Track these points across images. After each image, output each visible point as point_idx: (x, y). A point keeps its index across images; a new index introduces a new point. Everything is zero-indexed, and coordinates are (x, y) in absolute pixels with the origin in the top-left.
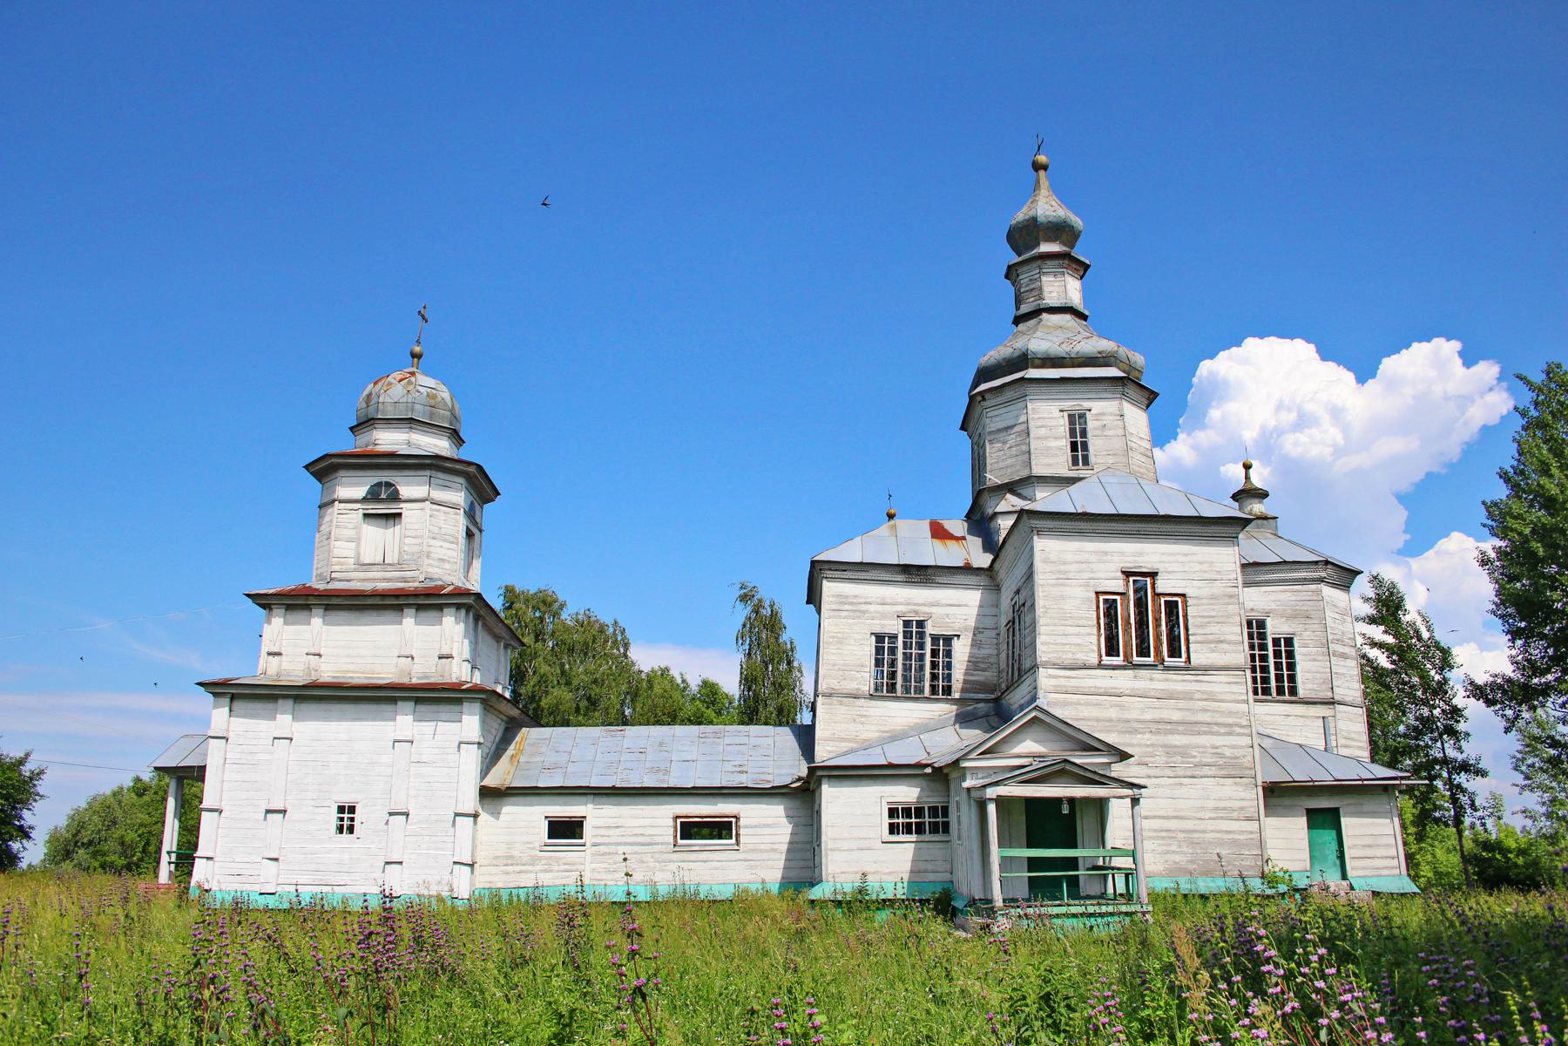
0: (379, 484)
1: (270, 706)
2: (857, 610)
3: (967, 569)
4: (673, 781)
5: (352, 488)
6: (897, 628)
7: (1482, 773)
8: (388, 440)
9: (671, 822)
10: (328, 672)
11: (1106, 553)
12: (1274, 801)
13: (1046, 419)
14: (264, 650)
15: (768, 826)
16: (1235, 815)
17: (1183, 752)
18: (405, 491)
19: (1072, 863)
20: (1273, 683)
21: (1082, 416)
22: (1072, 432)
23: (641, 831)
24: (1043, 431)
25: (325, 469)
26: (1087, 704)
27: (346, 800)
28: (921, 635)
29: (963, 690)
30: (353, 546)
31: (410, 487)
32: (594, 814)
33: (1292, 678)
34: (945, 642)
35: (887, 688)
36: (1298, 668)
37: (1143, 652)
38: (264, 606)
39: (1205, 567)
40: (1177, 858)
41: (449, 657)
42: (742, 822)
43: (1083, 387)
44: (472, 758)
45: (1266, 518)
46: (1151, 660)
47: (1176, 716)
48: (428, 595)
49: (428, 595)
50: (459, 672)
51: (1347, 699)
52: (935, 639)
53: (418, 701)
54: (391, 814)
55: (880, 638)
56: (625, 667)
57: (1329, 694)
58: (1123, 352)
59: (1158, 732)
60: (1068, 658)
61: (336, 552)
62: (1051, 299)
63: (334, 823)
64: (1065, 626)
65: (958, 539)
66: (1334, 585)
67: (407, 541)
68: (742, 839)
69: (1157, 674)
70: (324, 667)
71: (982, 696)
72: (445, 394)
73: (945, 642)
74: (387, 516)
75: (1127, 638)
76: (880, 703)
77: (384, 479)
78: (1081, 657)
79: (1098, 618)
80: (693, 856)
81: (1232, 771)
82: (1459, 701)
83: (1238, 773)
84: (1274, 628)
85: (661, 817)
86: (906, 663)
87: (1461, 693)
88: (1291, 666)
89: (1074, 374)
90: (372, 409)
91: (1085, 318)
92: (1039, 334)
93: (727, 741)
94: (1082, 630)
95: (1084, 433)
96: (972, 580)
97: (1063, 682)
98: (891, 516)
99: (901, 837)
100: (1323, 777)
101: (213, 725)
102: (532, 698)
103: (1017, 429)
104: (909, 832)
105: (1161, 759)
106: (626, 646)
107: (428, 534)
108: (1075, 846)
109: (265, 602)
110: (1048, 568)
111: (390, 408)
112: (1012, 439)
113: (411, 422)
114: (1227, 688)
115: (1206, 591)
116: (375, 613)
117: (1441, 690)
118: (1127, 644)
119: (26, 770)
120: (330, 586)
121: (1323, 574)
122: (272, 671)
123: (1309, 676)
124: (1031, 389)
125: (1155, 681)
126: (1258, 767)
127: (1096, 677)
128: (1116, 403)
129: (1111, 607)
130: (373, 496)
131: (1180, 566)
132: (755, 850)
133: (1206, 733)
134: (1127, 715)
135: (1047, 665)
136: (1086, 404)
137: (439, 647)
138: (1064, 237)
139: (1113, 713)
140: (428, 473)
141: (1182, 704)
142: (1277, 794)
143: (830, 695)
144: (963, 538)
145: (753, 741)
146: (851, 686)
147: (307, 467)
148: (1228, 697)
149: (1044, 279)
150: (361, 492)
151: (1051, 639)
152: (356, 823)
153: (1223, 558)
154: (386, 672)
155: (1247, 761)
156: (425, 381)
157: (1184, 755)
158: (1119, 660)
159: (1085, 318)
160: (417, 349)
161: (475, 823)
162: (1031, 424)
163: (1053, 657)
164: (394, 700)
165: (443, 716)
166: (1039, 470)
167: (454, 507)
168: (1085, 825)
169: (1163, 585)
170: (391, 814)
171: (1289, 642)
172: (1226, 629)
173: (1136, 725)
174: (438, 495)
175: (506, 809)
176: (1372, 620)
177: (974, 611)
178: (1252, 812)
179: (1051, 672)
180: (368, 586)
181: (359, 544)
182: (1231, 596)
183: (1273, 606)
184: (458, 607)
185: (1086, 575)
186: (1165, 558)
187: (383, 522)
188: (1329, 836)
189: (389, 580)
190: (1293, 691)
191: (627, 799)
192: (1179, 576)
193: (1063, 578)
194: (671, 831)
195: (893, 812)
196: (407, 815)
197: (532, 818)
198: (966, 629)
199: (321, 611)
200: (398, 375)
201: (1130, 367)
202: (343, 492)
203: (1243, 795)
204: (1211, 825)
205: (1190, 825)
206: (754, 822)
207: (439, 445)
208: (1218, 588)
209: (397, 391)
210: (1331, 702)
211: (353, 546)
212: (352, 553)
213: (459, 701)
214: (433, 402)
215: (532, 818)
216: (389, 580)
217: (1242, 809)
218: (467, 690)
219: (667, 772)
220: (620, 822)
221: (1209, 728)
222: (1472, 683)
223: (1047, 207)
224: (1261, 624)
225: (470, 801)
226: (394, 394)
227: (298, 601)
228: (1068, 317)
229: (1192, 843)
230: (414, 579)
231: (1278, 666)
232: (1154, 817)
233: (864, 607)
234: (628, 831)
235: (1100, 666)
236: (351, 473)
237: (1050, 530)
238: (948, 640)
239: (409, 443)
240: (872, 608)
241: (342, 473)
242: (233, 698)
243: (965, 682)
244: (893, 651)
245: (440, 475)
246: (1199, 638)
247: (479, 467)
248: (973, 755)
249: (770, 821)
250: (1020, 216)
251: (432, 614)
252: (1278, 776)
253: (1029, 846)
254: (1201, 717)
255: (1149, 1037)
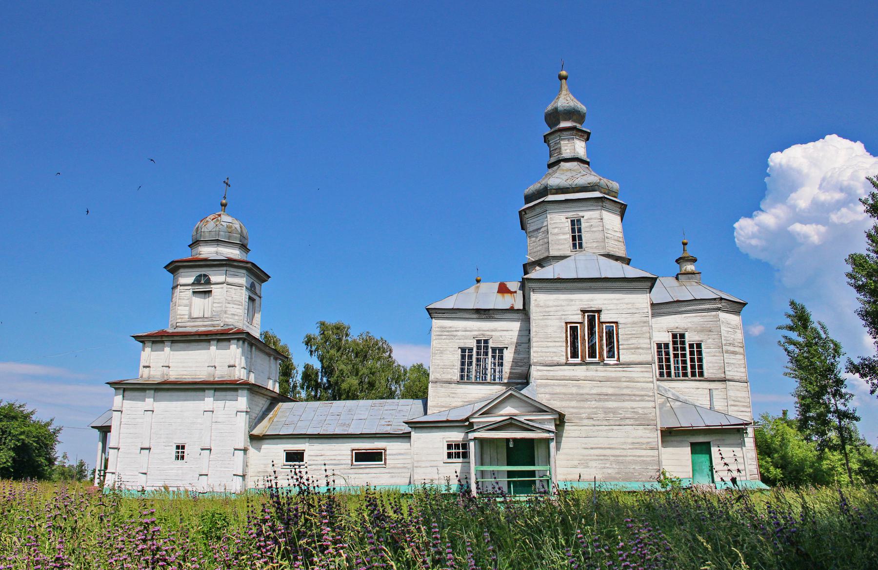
0: (200, 276)
1: (143, 394)
2: (451, 334)
3: (512, 310)
4: (351, 431)
5: (187, 278)
6: (473, 344)
7: (857, 419)
8: (207, 251)
9: (350, 453)
10: (173, 375)
11: (572, 300)
12: (669, 438)
13: (558, 223)
14: (142, 365)
15: (400, 454)
16: (644, 446)
17: (614, 411)
18: (213, 279)
19: (532, 474)
20: (689, 370)
21: (579, 221)
22: (573, 230)
23: (333, 458)
24: (556, 231)
25: (174, 268)
26: (559, 385)
27: (180, 442)
28: (486, 347)
29: (509, 378)
30: (188, 309)
31: (216, 277)
32: (310, 449)
33: (701, 367)
34: (499, 352)
35: (464, 378)
36: (704, 361)
37: (592, 355)
38: (141, 342)
39: (630, 306)
40: (610, 471)
41: (234, 366)
42: (388, 452)
43: (579, 204)
44: (242, 422)
45: (694, 274)
46: (597, 360)
47: (610, 391)
48: (222, 334)
49: (222, 334)
50: (240, 374)
51: (736, 378)
52: (494, 350)
53: (216, 390)
54: (202, 449)
55: (463, 350)
56: (389, 364)
57: (723, 375)
58: (604, 181)
59: (600, 400)
60: (548, 360)
61: (179, 312)
62: (567, 152)
63: (174, 455)
64: (548, 342)
65: (511, 293)
66: (727, 312)
67: (215, 305)
68: (388, 462)
69: (600, 368)
70: (171, 373)
71: (520, 381)
72: (237, 225)
73: (499, 352)
74: (205, 292)
75: (583, 347)
76: (463, 386)
77: (203, 273)
78: (556, 359)
79: (567, 337)
80: (361, 471)
81: (643, 421)
82: (843, 375)
83: (646, 422)
84: (690, 338)
85: (344, 450)
86: (475, 361)
87: (844, 370)
88: (700, 360)
89: (575, 197)
90: (198, 235)
91: (588, 163)
92: (557, 175)
93: (386, 408)
94: (557, 344)
95: (580, 231)
96: (515, 316)
97: (545, 373)
98: (478, 281)
99: (454, 460)
100: (700, 424)
101: (115, 404)
102: (336, 383)
103: (542, 230)
104: (459, 457)
105: (601, 416)
106: (391, 351)
107: (226, 301)
108: (534, 465)
109: (142, 339)
110: (538, 310)
111: (207, 234)
112: (540, 235)
113: (217, 242)
114: (641, 375)
115: (630, 320)
116: (196, 344)
117: (831, 369)
118: (583, 351)
119: (51, 428)
120: (176, 330)
121: (720, 306)
122: (145, 375)
123: (710, 365)
124: (549, 207)
125: (598, 372)
126: (658, 419)
127: (565, 370)
128: (598, 212)
129: (574, 330)
130: (197, 282)
131: (613, 306)
132: (394, 468)
133: (628, 400)
134: (581, 391)
135: (536, 364)
136: (581, 214)
137: (228, 361)
138: (575, 117)
139: (574, 390)
140: (225, 268)
141: (614, 384)
142: (670, 435)
143: (436, 382)
144: (515, 292)
145: (400, 408)
146: (448, 377)
147: (165, 267)
148: (641, 380)
149: (562, 142)
150: (191, 280)
151: (539, 350)
152: (185, 454)
153: (641, 301)
154: (202, 374)
155: (651, 416)
156: (226, 219)
157: (614, 413)
158: (578, 360)
159: (588, 163)
160: (224, 201)
161: (245, 454)
162: (549, 226)
163: (540, 359)
164: (204, 390)
165: (228, 397)
166: (553, 253)
167: (240, 286)
168: (539, 453)
169: (604, 318)
170: (202, 449)
171: (699, 346)
172: (641, 341)
173: (587, 396)
174: (230, 280)
175: (264, 447)
176: (791, 329)
177: (516, 333)
178: (654, 445)
179: (538, 368)
180: (194, 330)
181: (190, 308)
182: (645, 322)
183: (690, 325)
184: (238, 339)
185: (560, 313)
186: (606, 302)
187: (203, 295)
188: (704, 458)
189: (205, 326)
190: (701, 374)
191: (326, 441)
192: (614, 312)
193: (547, 315)
194: (350, 457)
195: (449, 447)
196: (210, 450)
197: (277, 451)
198: (511, 344)
199: (169, 344)
200: (212, 217)
201: (609, 191)
202: (182, 280)
203: (649, 435)
204: (630, 452)
205: (617, 452)
206: (394, 452)
207: (234, 253)
208: (637, 318)
209: (211, 225)
210: (724, 380)
211: (188, 309)
212: (187, 313)
213: (236, 390)
214: (230, 230)
215: (277, 451)
216: (205, 326)
217: (648, 443)
218: (240, 384)
219: (349, 425)
220: (323, 453)
221: (631, 397)
222: (852, 363)
223: (565, 100)
224: (682, 336)
225: (241, 440)
226: (209, 227)
227: (158, 339)
228: (575, 163)
229: (618, 463)
230: (218, 325)
231: (692, 360)
232: (597, 448)
233: (455, 333)
234: (327, 458)
235: (566, 364)
236: (186, 270)
237: (540, 288)
238: (501, 350)
239: (217, 253)
240: (459, 333)
241: (181, 270)
242: (124, 390)
243: (510, 373)
244: (470, 357)
245: (232, 269)
246: (625, 347)
247: (253, 264)
248: (477, 415)
249: (402, 451)
250: (550, 108)
251: (225, 344)
252: (672, 423)
253: (508, 465)
254: (625, 391)
255: (229, 567)
